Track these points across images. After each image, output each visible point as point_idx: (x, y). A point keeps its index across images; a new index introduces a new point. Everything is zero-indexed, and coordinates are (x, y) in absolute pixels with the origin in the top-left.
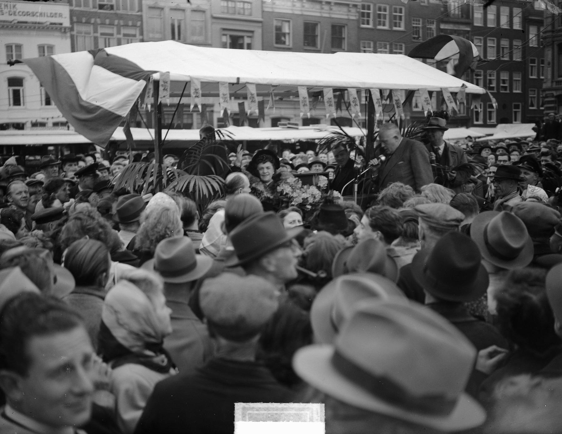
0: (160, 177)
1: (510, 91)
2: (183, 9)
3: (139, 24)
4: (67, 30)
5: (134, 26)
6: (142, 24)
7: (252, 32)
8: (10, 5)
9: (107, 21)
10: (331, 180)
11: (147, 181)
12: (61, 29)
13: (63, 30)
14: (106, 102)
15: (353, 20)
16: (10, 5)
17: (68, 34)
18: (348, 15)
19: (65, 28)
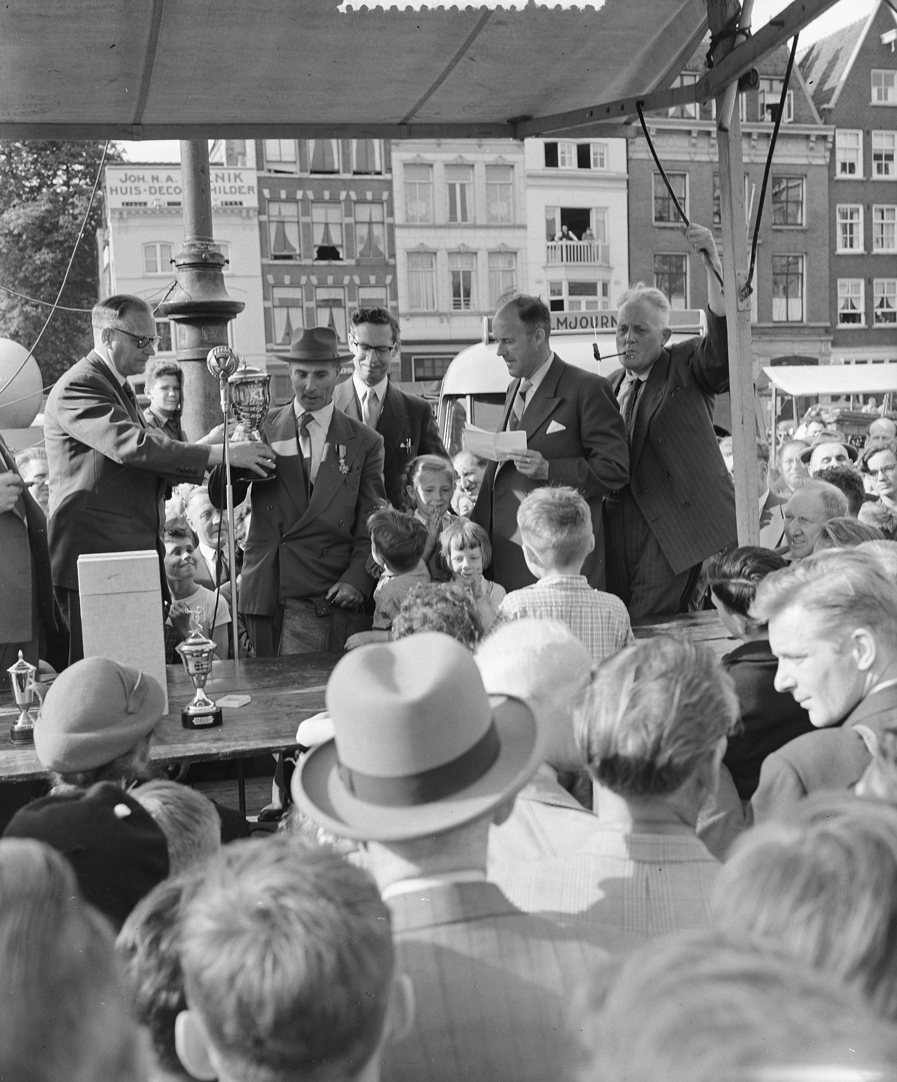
0: (646, 727)
1: (866, 323)
2: (430, 163)
3: (385, 195)
4: (252, 213)
5: (377, 201)
6: (391, 196)
7: (179, 204)
8: (229, 175)
9: (327, 195)
10: (171, 772)
11: (881, 759)
12: (240, 212)
13: (244, 213)
14: (670, 379)
15: (819, 166)
16: (229, 175)
17: (255, 222)
18: (807, 157)
19: (248, 210)
